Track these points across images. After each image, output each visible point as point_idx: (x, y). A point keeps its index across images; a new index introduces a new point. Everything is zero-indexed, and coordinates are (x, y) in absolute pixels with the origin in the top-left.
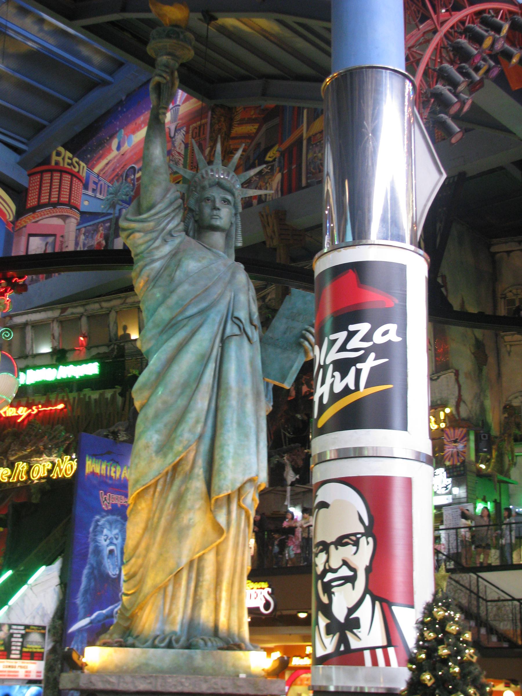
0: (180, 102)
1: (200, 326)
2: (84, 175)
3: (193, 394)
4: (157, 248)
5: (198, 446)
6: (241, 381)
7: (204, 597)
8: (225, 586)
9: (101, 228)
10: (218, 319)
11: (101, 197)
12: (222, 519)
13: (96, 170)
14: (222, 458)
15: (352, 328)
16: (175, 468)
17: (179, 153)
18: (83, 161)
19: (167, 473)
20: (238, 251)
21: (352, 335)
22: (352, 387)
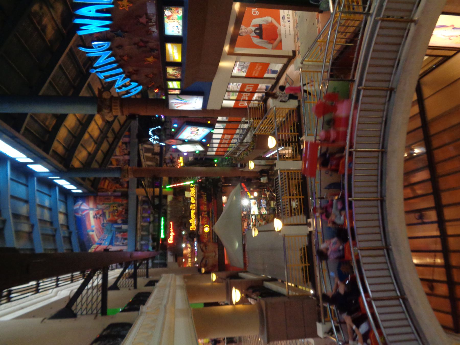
11: (106, 237)
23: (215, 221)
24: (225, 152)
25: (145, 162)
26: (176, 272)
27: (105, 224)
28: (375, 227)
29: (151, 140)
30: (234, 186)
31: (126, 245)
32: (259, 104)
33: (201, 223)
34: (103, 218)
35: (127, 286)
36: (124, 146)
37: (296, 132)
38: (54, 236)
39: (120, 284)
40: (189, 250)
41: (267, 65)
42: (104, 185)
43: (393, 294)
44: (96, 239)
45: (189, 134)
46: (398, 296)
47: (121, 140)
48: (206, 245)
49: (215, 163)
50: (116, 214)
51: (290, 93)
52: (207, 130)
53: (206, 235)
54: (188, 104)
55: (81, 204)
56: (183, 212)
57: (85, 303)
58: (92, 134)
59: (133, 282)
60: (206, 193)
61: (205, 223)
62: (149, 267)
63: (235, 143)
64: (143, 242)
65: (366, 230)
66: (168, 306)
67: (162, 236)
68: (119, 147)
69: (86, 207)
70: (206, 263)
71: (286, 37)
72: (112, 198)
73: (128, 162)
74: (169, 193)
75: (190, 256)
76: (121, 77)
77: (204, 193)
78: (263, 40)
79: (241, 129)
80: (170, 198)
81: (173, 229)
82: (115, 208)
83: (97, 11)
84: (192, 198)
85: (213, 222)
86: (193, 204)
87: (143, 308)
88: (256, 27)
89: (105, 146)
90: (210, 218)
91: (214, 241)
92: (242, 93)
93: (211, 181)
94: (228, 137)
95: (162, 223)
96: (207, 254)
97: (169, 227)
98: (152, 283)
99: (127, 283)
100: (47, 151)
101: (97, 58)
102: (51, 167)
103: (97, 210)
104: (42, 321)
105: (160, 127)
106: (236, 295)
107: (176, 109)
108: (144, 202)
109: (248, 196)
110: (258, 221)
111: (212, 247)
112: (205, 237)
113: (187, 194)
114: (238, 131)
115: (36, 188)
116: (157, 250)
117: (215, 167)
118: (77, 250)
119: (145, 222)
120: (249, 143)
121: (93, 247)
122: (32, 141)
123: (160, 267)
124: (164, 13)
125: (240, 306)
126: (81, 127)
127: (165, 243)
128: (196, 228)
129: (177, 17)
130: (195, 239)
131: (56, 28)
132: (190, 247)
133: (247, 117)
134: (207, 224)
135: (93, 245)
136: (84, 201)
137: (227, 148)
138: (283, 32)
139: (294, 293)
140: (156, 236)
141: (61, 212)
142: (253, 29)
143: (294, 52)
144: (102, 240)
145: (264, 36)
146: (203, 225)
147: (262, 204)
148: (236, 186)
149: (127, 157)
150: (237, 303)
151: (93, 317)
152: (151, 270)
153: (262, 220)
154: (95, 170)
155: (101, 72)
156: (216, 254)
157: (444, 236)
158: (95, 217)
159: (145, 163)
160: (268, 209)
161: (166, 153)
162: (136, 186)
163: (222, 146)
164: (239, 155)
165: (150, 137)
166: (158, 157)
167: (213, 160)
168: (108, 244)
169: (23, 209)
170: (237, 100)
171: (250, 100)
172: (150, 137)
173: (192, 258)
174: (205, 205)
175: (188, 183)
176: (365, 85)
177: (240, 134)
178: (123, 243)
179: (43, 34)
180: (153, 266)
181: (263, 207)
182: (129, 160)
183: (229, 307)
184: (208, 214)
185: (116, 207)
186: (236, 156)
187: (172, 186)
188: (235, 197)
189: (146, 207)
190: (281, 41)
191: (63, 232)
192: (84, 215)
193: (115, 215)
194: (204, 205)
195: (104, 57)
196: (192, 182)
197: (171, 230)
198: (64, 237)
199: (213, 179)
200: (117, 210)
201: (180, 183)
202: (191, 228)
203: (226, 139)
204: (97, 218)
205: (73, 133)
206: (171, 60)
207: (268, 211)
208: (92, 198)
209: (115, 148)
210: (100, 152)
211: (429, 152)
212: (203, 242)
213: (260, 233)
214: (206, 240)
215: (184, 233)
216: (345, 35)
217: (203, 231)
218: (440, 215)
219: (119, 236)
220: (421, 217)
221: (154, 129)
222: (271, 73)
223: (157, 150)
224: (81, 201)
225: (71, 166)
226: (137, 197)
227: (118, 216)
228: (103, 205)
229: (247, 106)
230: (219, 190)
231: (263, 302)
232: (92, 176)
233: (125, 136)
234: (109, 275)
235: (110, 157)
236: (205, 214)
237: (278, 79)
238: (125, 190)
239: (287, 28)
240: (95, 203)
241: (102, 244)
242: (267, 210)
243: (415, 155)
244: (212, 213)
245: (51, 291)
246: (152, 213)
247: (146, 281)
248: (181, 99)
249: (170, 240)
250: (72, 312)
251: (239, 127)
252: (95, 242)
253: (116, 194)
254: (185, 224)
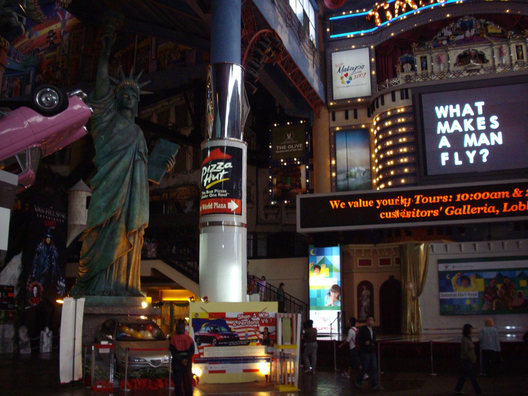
0: (67, 18)
1: (124, 155)
2: (8, 48)
3: (121, 185)
4: (104, 117)
5: (122, 209)
6: (141, 181)
7: (122, 274)
8: (131, 270)
9: (18, 79)
10: (132, 152)
11: (19, 62)
12: (131, 241)
13: (16, 46)
14: (134, 215)
15: (218, 163)
16: (112, 218)
17: (66, 46)
18: (7, 40)
19: (108, 220)
20: (136, 118)
21: (218, 165)
22: (218, 179)
50: (51, 69)
51: (300, 228)
82: (60, 66)
185: (63, 66)
193: (49, 68)
204: (49, 37)
219: (16, 83)
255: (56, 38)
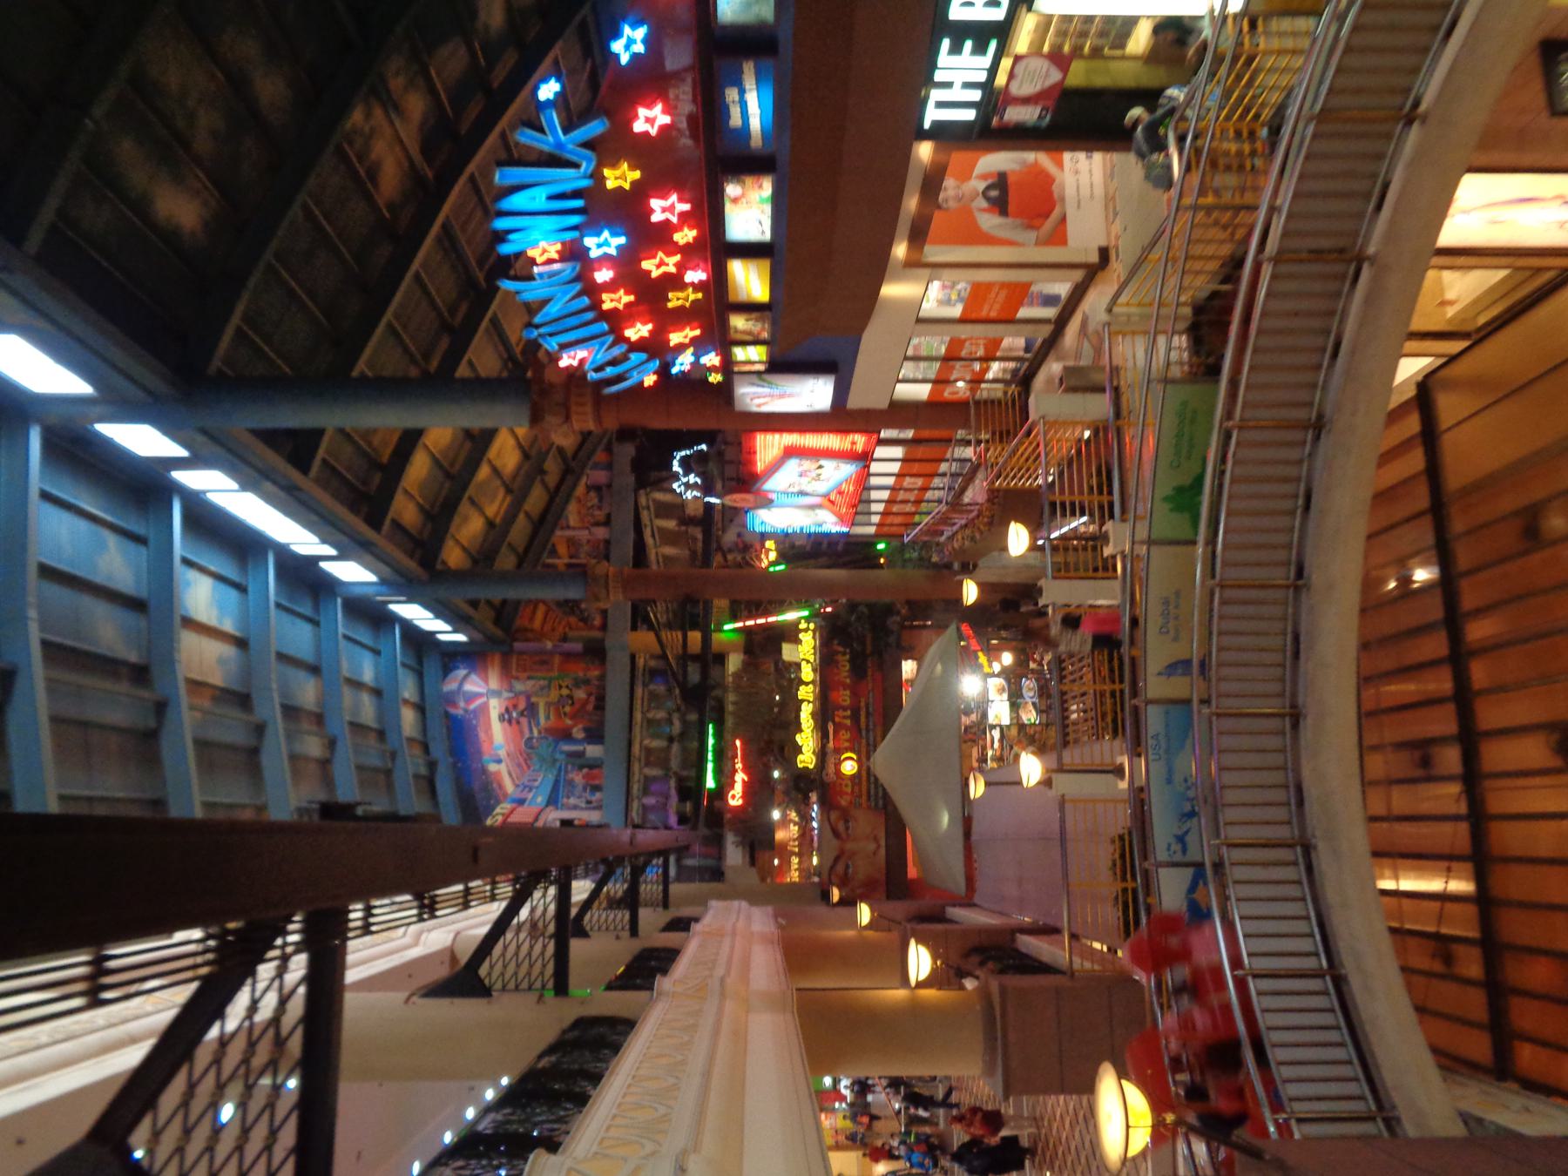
11: (540, 779)
23: (879, 739)
24: (906, 525)
25: (656, 546)
26: (754, 898)
27: (534, 741)
28: (1275, 786)
29: (679, 486)
30: (941, 627)
31: (599, 808)
32: (1005, 393)
33: (831, 744)
34: (530, 723)
35: (612, 927)
36: (593, 498)
37: (1105, 493)
38: (388, 773)
39: (591, 921)
40: (794, 829)
41: (1027, 286)
42: (532, 619)
43: (1309, 963)
44: (509, 787)
45: (794, 478)
46: (1321, 968)
47: (584, 480)
48: (846, 817)
49: (880, 554)
50: (568, 709)
52: (849, 466)
53: (846, 786)
54: (790, 395)
55: (465, 677)
56: (776, 710)
57: (511, 959)
58: (498, 463)
59: (627, 917)
60: (848, 651)
61: (847, 744)
62: (671, 880)
63: (940, 501)
64: (650, 801)
65: (1248, 796)
66: (729, 981)
67: (710, 783)
68: (579, 501)
69: (480, 686)
70: (846, 874)
71: (1079, 206)
72: (557, 660)
73: (604, 551)
74: (732, 647)
75: (797, 850)
76: (602, 344)
77: (841, 649)
78: (1009, 220)
79: (954, 460)
80: (734, 662)
81: (742, 759)
82: (565, 692)
83: (551, 198)
84: (804, 663)
85: (871, 742)
86: (807, 684)
87: (663, 983)
88: (989, 181)
89: (536, 499)
90: (860, 730)
91: (873, 804)
92: (951, 363)
93: (865, 610)
94: (916, 483)
95: (711, 741)
96: (849, 846)
97: (730, 754)
98: (681, 925)
99: (521, 974)
100: (375, 522)
101: (545, 302)
102: (386, 570)
103: (511, 695)
104: (407, 1000)
105: (704, 447)
106: (920, 961)
107: (755, 409)
108: (653, 674)
109: (981, 666)
110: (1011, 748)
111: (866, 824)
112: (844, 789)
113: (788, 652)
114: (944, 467)
115: (341, 630)
116: (694, 828)
117: (881, 566)
118: (451, 815)
119: (655, 736)
120: (977, 504)
121: (498, 810)
122: (336, 496)
123: (702, 880)
124: (722, 191)
125: (930, 993)
126: (468, 445)
127: (717, 804)
128: (817, 760)
129: (758, 199)
130: (814, 797)
131: (406, 164)
132: (797, 819)
133: (970, 427)
134: (852, 750)
135: (498, 802)
136: (472, 669)
137: (914, 514)
138: (1070, 192)
139: (1088, 965)
140: (691, 784)
141: (406, 702)
142: (981, 186)
143: (1104, 253)
144: (527, 789)
145: (1011, 208)
146: (839, 751)
147: (1024, 691)
148: (946, 627)
149: (601, 533)
150: (920, 985)
151: (533, 996)
152: (675, 888)
153: (1025, 742)
154: (504, 578)
155: (551, 335)
156: (879, 847)
157: (1478, 817)
158: (506, 717)
159: (657, 551)
160: (1044, 708)
161: (724, 530)
162: (629, 624)
163: (895, 508)
164: (951, 538)
165: (676, 477)
166: (697, 533)
167: (875, 544)
168: (544, 804)
169: (307, 692)
170: (940, 382)
171: (977, 380)
172: (676, 477)
173: (804, 854)
174: (845, 687)
175: (790, 616)
176: (1241, 417)
177: (952, 475)
178: (589, 802)
179: (372, 190)
180: (679, 879)
181: (1026, 703)
182: (607, 542)
183: (901, 994)
184: (855, 717)
185: (567, 687)
186: (943, 539)
187: (740, 624)
188: (939, 667)
189: (660, 688)
190: (1063, 219)
191: (411, 764)
192: (475, 711)
194: (841, 688)
195: (561, 299)
196: (805, 613)
197: (737, 766)
198: (417, 776)
199: (870, 606)
200: (570, 697)
201: (767, 614)
202: (801, 762)
203: (911, 490)
204: (510, 722)
205: (445, 464)
206: (743, 296)
207: (1044, 716)
208: (497, 659)
209: (567, 502)
210: (521, 516)
211: (1447, 584)
212: (837, 807)
213: (993, 788)
214: (848, 798)
215: (776, 774)
216: (1233, 234)
217: (838, 772)
218: (1470, 757)
219: (578, 778)
220: (1426, 762)
221: (688, 452)
222: (1038, 305)
223: (698, 511)
224: (465, 668)
225: (439, 567)
226: (633, 657)
227: (573, 717)
228: (530, 683)
229: (968, 397)
230: (892, 639)
231: (994, 986)
232: (497, 593)
233: (596, 466)
234: (574, 891)
235: (552, 531)
236: (845, 717)
237: (1061, 323)
238: (597, 634)
239: (1084, 179)
240: (507, 674)
241: (527, 802)
242: (1039, 712)
243: (1416, 585)
244: (868, 714)
245: (402, 930)
246: (678, 710)
247: (664, 917)
248: (770, 383)
249: (733, 797)
250: (481, 981)
251: (948, 455)
252: (506, 795)
253: (567, 646)
254: (782, 749)
255: (515, 706)
